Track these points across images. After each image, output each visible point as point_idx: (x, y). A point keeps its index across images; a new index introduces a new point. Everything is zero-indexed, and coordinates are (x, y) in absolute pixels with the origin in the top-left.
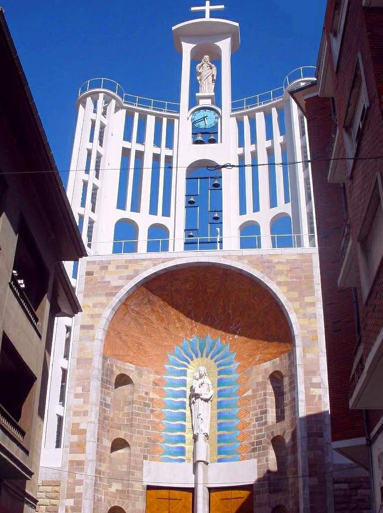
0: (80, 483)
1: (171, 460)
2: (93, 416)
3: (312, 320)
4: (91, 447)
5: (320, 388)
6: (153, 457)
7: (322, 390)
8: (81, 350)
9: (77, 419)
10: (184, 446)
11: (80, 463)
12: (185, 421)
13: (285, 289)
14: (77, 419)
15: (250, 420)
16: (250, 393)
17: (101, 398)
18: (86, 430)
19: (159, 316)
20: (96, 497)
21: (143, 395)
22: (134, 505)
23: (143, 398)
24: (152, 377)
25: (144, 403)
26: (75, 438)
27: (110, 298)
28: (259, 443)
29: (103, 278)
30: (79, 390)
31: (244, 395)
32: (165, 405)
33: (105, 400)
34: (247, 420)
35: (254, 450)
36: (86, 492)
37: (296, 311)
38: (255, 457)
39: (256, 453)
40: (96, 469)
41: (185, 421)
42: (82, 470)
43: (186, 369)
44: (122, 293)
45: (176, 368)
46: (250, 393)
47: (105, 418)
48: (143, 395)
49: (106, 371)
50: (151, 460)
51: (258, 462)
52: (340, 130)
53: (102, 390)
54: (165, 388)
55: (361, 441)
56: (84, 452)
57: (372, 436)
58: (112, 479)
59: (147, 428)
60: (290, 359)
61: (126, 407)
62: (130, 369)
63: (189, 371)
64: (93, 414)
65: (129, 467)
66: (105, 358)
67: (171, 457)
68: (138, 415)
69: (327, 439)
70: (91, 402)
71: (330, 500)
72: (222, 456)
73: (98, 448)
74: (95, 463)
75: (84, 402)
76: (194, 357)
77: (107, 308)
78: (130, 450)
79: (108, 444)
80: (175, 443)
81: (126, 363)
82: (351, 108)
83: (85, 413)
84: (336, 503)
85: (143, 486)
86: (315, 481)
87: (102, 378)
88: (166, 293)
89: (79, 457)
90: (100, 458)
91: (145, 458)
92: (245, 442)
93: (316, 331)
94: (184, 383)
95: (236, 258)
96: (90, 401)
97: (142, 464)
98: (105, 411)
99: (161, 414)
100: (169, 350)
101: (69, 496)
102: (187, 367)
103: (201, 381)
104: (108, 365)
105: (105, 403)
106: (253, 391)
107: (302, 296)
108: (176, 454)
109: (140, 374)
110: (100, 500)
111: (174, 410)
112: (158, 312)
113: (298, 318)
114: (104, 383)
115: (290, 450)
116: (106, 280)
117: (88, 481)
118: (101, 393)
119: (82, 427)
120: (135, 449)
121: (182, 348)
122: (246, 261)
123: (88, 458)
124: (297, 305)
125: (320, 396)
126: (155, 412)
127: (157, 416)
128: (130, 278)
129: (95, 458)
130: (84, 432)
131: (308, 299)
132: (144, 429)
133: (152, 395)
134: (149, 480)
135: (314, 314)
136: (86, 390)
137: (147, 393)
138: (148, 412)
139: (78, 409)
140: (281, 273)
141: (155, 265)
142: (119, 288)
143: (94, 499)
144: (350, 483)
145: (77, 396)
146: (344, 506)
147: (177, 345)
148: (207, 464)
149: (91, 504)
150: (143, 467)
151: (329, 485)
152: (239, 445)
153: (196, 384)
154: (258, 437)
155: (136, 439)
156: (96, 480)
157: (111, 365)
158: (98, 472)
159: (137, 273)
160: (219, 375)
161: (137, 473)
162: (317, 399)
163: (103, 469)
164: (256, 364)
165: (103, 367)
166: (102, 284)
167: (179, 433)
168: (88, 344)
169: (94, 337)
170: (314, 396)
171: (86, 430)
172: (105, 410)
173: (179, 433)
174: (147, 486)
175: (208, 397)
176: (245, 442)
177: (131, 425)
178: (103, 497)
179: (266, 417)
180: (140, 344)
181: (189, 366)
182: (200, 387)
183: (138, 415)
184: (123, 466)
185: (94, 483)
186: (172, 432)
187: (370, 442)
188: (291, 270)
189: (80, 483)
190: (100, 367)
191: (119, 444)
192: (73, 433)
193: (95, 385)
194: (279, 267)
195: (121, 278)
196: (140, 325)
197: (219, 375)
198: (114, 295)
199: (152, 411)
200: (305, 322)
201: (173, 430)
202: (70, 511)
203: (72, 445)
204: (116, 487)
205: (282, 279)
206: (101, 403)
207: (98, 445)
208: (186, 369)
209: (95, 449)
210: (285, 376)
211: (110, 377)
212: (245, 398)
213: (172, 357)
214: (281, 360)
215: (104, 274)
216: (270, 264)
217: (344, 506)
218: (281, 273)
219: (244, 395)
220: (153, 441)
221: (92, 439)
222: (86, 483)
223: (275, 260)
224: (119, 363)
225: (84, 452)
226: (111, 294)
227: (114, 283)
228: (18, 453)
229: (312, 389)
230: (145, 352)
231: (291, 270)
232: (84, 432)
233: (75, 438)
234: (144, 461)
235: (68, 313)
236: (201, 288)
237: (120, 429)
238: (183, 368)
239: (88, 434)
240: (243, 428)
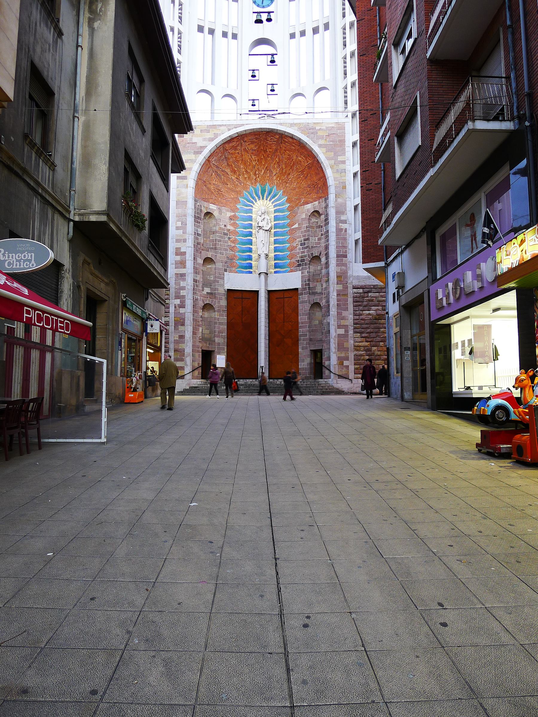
0: (183, 288)
1: (243, 272)
2: (190, 242)
3: (343, 174)
4: (190, 264)
5: (346, 223)
6: (231, 270)
7: (348, 225)
8: (178, 195)
9: (178, 245)
10: (251, 262)
11: (183, 275)
12: (252, 245)
13: (324, 150)
14: (178, 245)
15: (297, 245)
16: (296, 226)
17: (195, 229)
18: (186, 252)
19: (233, 169)
20: (194, 298)
21: (223, 227)
22: (219, 302)
23: (223, 230)
24: (229, 214)
25: (224, 233)
26: (178, 258)
27: (197, 155)
28: (303, 261)
29: (191, 139)
30: (179, 224)
31: (292, 228)
32: (235, 233)
33: (197, 231)
34: (295, 245)
35: (299, 265)
36: (188, 293)
37: (332, 167)
38: (299, 270)
39: (301, 268)
40: (194, 279)
41: (252, 245)
42: (184, 280)
43: (251, 208)
44: (206, 153)
45: (245, 207)
46: (296, 226)
47: (198, 244)
48: (223, 227)
49: (197, 210)
50: (230, 272)
51: (302, 273)
52: (389, 44)
53: (195, 224)
54: (237, 222)
55: (382, 264)
56: (185, 267)
57: (389, 262)
58: (205, 285)
59: (226, 250)
60: (326, 202)
61: (211, 236)
62: (213, 207)
63: (254, 210)
64: (190, 240)
65: (215, 277)
66: (196, 201)
67: (243, 270)
68: (220, 241)
69: (349, 259)
70: (188, 232)
71: (350, 300)
72: (277, 270)
73: (194, 264)
74: (193, 274)
75: (183, 233)
76: (257, 200)
77: (195, 163)
78: (216, 266)
79: (200, 261)
80: (246, 261)
81: (210, 204)
82: (400, 30)
83: (185, 240)
84: (354, 302)
85: (224, 289)
86: (340, 287)
87: (195, 216)
88: (237, 152)
89: (182, 271)
90: (196, 271)
91: (226, 271)
92: (293, 260)
93: (345, 182)
94: (250, 219)
95: (289, 125)
96: (187, 232)
97: (224, 275)
98: (197, 239)
99: (236, 240)
100: (240, 194)
101: (177, 297)
102: (252, 207)
103: (263, 217)
104: (198, 206)
105: (198, 233)
106: (299, 224)
107: (336, 155)
108: (246, 268)
109: (220, 212)
110: (197, 300)
111: (244, 237)
112: (232, 166)
113: (333, 173)
114: (197, 219)
115: (324, 266)
116: (194, 141)
117: (189, 287)
118: (195, 226)
119: (182, 250)
120: (219, 265)
121: (249, 193)
122: (296, 128)
123: (188, 272)
124: (333, 162)
125: (346, 229)
126: (231, 239)
127: (233, 242)
128: (212, 140)
129: (193, 272)
130: (184, 253)
131: (340, 158)
132: (225, 251)
133: (229, 227)
134: (228, 286)
135: (344, 169)
136: (184, 224)
137: (225, 226)
138: (227, 239)
139: (178, 238)
140: (322, 137)
141: (229, 130)
142: (204, 147)
143: (193, 299)
144: (364, 289)
145: (178, 228)
146: (360, 303)
147: (245, 191)
148: (268, 274)
149: (191, 303)
150: (224, 277)
151: (351, 291)
152: (289, 262)
153: (259, 219)
154: (302, 257)
155: (220, 258)
156: (194, 286)
157: (200, 205)
158: (195, 281)
159: (216, 136)
160: (275, 213)
161: (221, 281)
162: (344, 231)
163: (198, 279)
164: (301, 205)
165: (195, 207)
166: (191, 144)
167: (248, 254)
168: (183, 190)
169: (187, 185)
170: (342, 229)
171: (186, 252)
172: (198, 238)
173: (248, 254)
174: (227, 289)
175: (268, 229)
176: (293, 260)
177: (215, 249)
178: (199, 298)
179: (308, 243)
180: (219, 190)
181: (254, 206)
182: (262, 221)
183: (220, 241)
184: (211, 277)
185: (193, 289)
186: (243, 253)
187: (388, 265)
188: (329, 136)
189: (183, 288)
190: (193, 208)
191: (208, 260)
192: (177, 254)
193: (190, 220)
194: (320, 133)
195: (204, 140)
196: (220, 176)
197: (275, 213)
198: (200, 153)
199: (229, 238)
200: (338, 175)
201: (244, 251)
202: (177, 308)
203: (176, 263)
204: (207, 290)
205: (322, 142)
206: (195, 233)
207: (194, 262)
208: (251, 208)
209: (193, 265)
210: (322, 214)
211: (200, 214)
212: (293, 229)
213: (241, 199)
214: (319, 203)
215: (192, 136)
216: (314, 130)
217: (360, 303)
218: (322, 137)
219: (292, 228)
220: (231, 259)
221: (190, 259)
222: (187, 288)
223: (318, 128)
224: (206, 204)
225: (185, 267)
226: (199, 153)
227: (199, 144)
228: (162, 271)
229: (340, 224)
230: (223, 196)
231: (329, 136)
232: (184, 253)
233: (178, 258)
234: (225, 272)
235: (176, 170)
236: (262, 148)
237: (208, 251)
238: (250, 208)
239: (187, 255)
240: (292, 250)
